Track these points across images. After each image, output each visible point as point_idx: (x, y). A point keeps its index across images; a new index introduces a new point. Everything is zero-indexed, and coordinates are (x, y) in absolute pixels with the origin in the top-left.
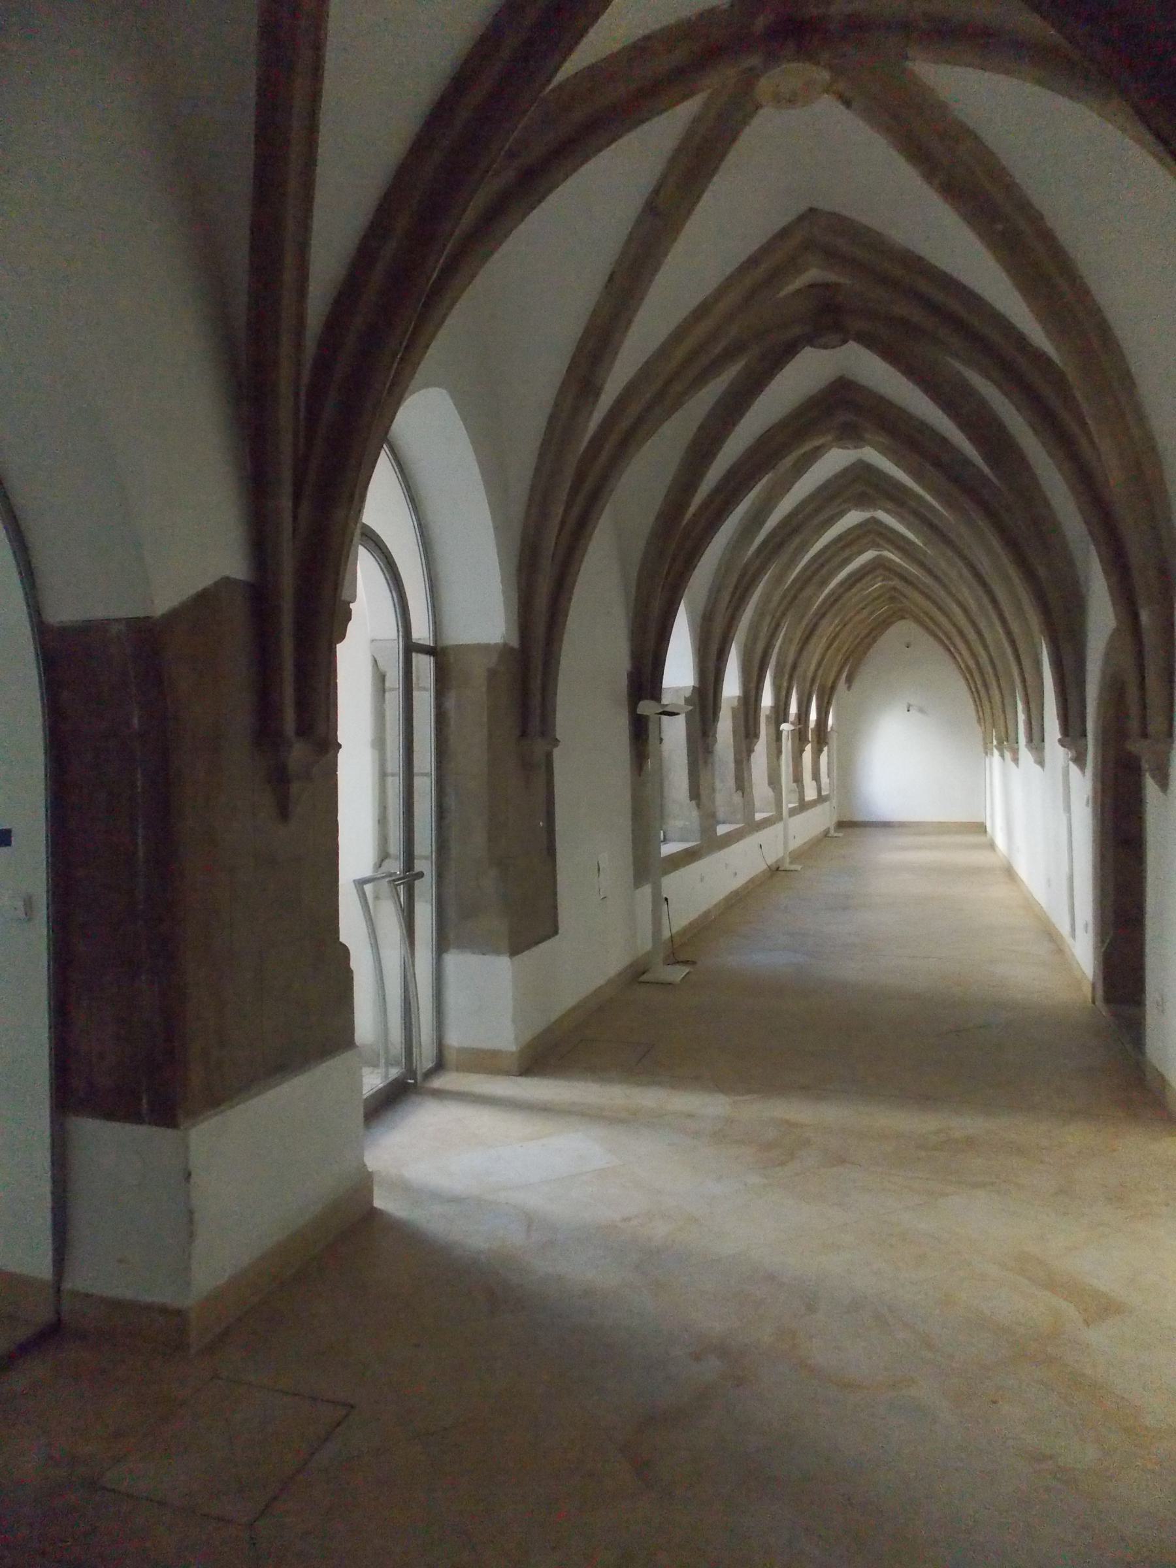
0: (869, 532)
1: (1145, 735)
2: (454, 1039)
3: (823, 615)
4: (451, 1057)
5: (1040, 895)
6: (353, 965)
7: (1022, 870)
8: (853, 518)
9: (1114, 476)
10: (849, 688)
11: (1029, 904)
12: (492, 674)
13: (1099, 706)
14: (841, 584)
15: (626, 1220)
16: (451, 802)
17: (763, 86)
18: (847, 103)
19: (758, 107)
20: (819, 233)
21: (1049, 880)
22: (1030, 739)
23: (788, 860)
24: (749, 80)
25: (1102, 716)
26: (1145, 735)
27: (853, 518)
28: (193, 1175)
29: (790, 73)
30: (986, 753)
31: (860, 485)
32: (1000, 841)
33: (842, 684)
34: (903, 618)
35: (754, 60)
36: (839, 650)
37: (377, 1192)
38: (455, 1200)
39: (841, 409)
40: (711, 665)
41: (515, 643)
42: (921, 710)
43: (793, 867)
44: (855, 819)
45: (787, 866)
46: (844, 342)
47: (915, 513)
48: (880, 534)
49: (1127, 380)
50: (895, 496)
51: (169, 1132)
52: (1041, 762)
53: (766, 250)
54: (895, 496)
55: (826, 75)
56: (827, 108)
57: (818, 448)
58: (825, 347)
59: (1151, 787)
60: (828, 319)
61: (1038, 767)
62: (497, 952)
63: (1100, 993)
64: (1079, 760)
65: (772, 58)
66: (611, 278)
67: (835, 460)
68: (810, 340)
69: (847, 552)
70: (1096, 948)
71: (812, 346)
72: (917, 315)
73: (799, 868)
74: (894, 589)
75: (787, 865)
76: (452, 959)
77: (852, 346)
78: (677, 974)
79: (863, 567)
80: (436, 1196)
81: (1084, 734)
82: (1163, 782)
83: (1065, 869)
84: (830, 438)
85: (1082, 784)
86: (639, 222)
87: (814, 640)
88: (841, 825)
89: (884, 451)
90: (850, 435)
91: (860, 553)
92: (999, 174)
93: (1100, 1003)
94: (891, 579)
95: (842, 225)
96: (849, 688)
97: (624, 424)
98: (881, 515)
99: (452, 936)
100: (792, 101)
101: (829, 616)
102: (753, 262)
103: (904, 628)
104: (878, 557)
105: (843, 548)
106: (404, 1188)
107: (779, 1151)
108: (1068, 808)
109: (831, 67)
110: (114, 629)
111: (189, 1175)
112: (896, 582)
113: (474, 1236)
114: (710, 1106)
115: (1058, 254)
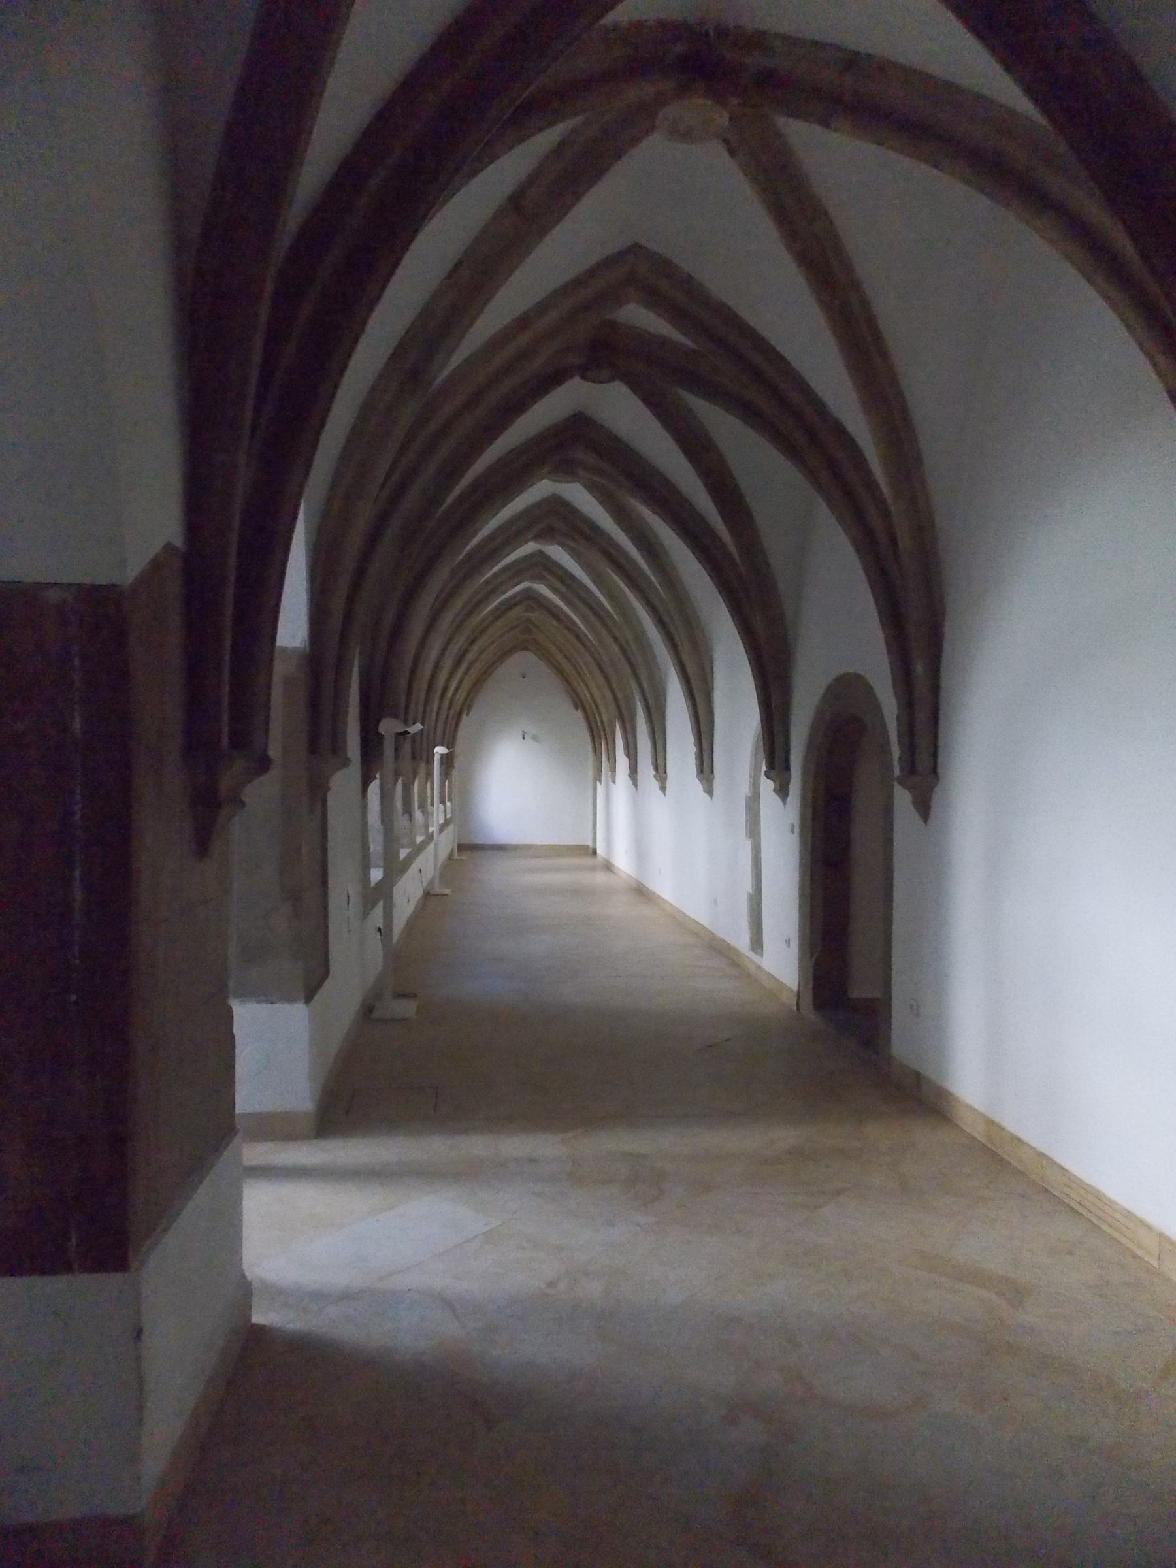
5: (698, 910)
6: (235, 1031)
7: (664, 887)
11: (679, 921)
15: (551, 1284)
17: (672, 111)
18: (732, 152)
20: (640, 270)
21: (715, 901)
23: (437, 881)
27: (530, 547)
28: (146, 1333)
29: (696, 109)
30: (598, 777)
32: (623, 861)
34: (526, 649)
38: (345, 1296)
42: (534, 738)
44: (480, 842)
51: (118, 1277)
52: (709, 792)
53: (592, 272)
62: (290, 1000)
63: (808, 998)
64: (782, 791)
66: (458, 266)
68: (584, 372)
70: (801, 959)
71: (583, 377)
73: (448, 891)
75: (438, 889)
78: (407, 1008)
79: (514, 596)
80: (320, 1296)
81: (787, 768)
83: (748, 886)
88: (462, 848)
95: (665, 266)
97: (433, 426)
100: (687, 136)
102: (577, 283)
103: (525, 659)
104: (528, 589)
106: (278, 1294)
107: (644, 1184)
108: (754, 831)
110: (53, 596)
111: (138, 1334)
113: (407, 1334)
114: (546, 1147)
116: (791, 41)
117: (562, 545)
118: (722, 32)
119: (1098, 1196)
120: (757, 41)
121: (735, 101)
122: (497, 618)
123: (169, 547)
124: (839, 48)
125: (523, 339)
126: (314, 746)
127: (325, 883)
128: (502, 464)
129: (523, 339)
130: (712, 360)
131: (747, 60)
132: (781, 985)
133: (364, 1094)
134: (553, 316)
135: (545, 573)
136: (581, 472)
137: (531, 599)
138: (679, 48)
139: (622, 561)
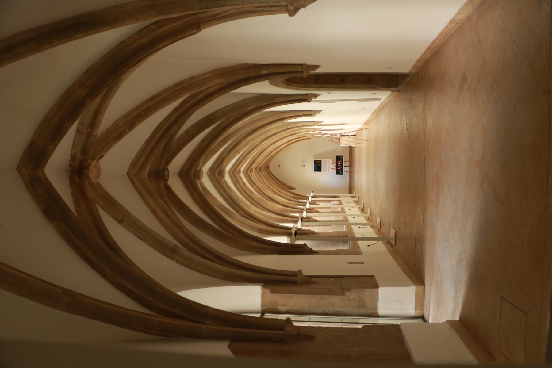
0: (233, 174)
1: (302, 72)
2: (412, 311)
3: (265, 194)
4: (419, 313)
5: (366, 117)
8: (227, 178)
9: (220, 81)
10: (295, 189)
12: (272, 292)
13: (298, 89)
14: (252, 186)
16: (320, 310)
17: (93, 180)
18: (102, 156)
19: (98, 183)
20: (134, 172)
22: (311, 115)
24: (90, 183)
25: (297, 88)
26: (302, 72)
29: (92, 172)
31: (217, 173)
33: (294, 191)
35: (87, 182)
36: (279, 191)
37: (455, 319)
39: (189, 175)
40: (279, 230)
41: (262, 284)
43: (362, 204)
45: (368, 215)
46: (168, 170)
47: (228, 154)
48: (235, 170)
49: (192, 78)
50: (221, 162)
53: (137, 189)
54: (221, 162)
55: (94, 161)
56: (102, 162)
57: (201, 186)
58: (168, 176)
59: (318, 71)
60: (160, 174)
61: (322, 112)
64: (316, 96)
65: (88, 177)
67: (206, 182)
69: (240, 182)
70: (380, 90)
72: (162, 145)
74: (256, 168)
76: (381, 312)
77: (169, 167)
81: (307, 94)
82: (317, 67)
84: (198, 182)
85: (324, 95)
86: (124, 226)
87: (273, 198)
88: (350, 192)
89: (205, 162)
90: (198, 174)
91: (241, 179)
92: (128, 114)
93: (400, 88)
94: (252, 169)
95: (134, 164)
96: (295, 189)
97: (187, 240)
98: (228, 168)
99: (372, 312)
100: (99, 172)
101: (264, 192)
102: (140, 193)
104: (243, 172)
105: (239, 184)
109: (93, 160)
112: (254, 166)
115: (153, 98)
116: (73, 147)
117: (225, 167)
118: (70, 165)
119: (441, 34)
120: (73, 157)
121: (89, 161)
122: (255, 184)
123: (229, 347)
124: (75, 135)
125: (159, 211)
126: (295, 283)
127: (343, 277)
128: (188, 131)
129: (159, 211)
130: (163, 144)
131: (78, 158)
132: (390, 95)
133: (414, 270)
134: (150, 201)
135: (237, 170)
136: (199, 168)
137: (247, 172)
138: (77, 180)
139: (231, 146)
